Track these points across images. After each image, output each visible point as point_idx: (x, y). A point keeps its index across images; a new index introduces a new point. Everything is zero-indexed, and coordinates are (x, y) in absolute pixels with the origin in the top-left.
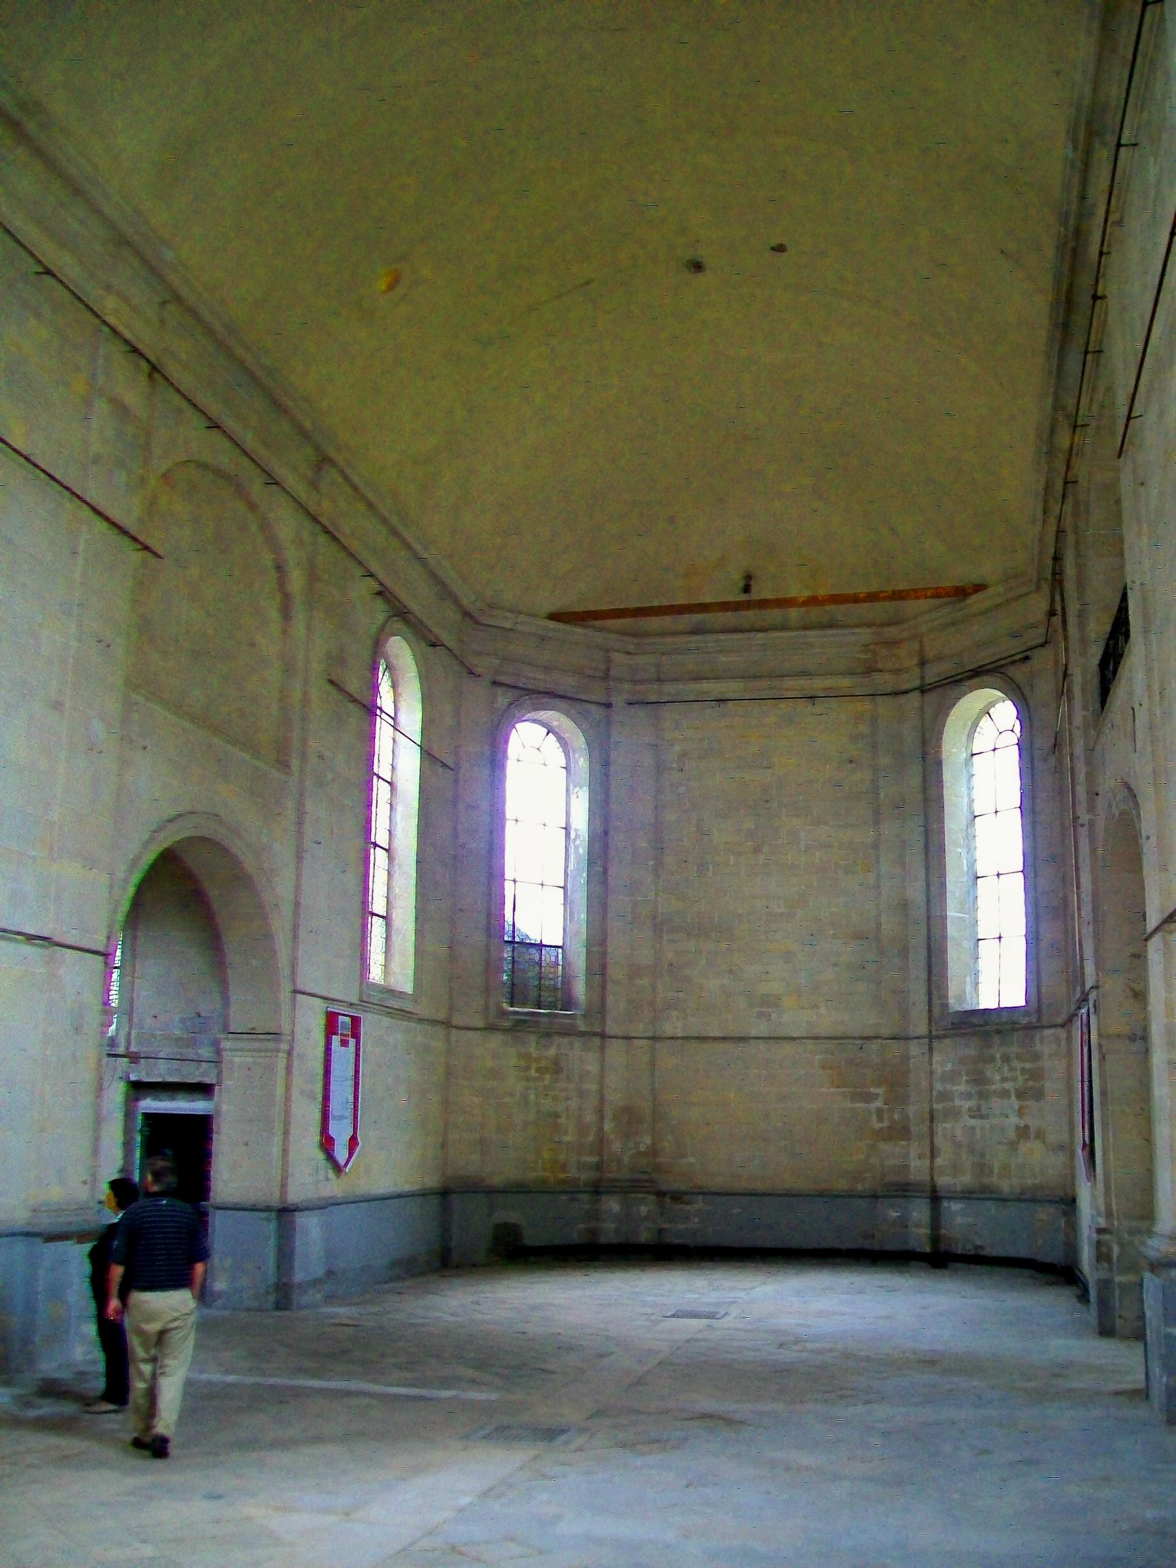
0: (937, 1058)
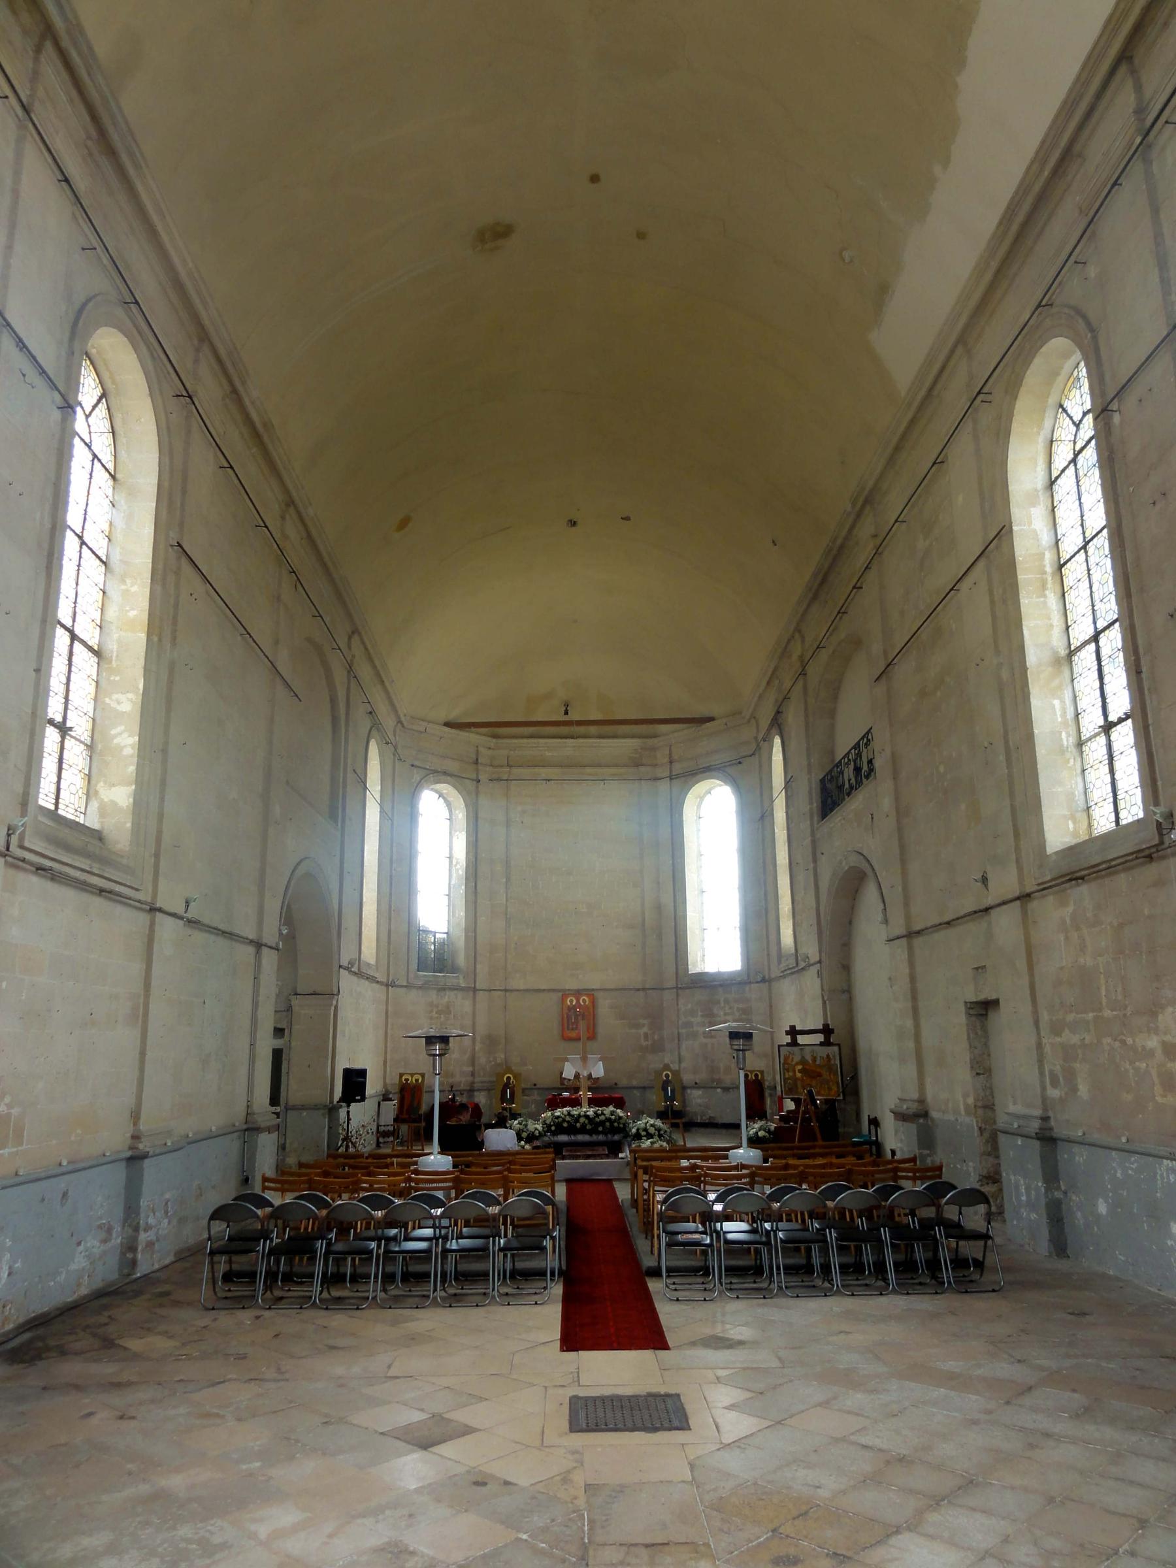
0: (681, 1001)
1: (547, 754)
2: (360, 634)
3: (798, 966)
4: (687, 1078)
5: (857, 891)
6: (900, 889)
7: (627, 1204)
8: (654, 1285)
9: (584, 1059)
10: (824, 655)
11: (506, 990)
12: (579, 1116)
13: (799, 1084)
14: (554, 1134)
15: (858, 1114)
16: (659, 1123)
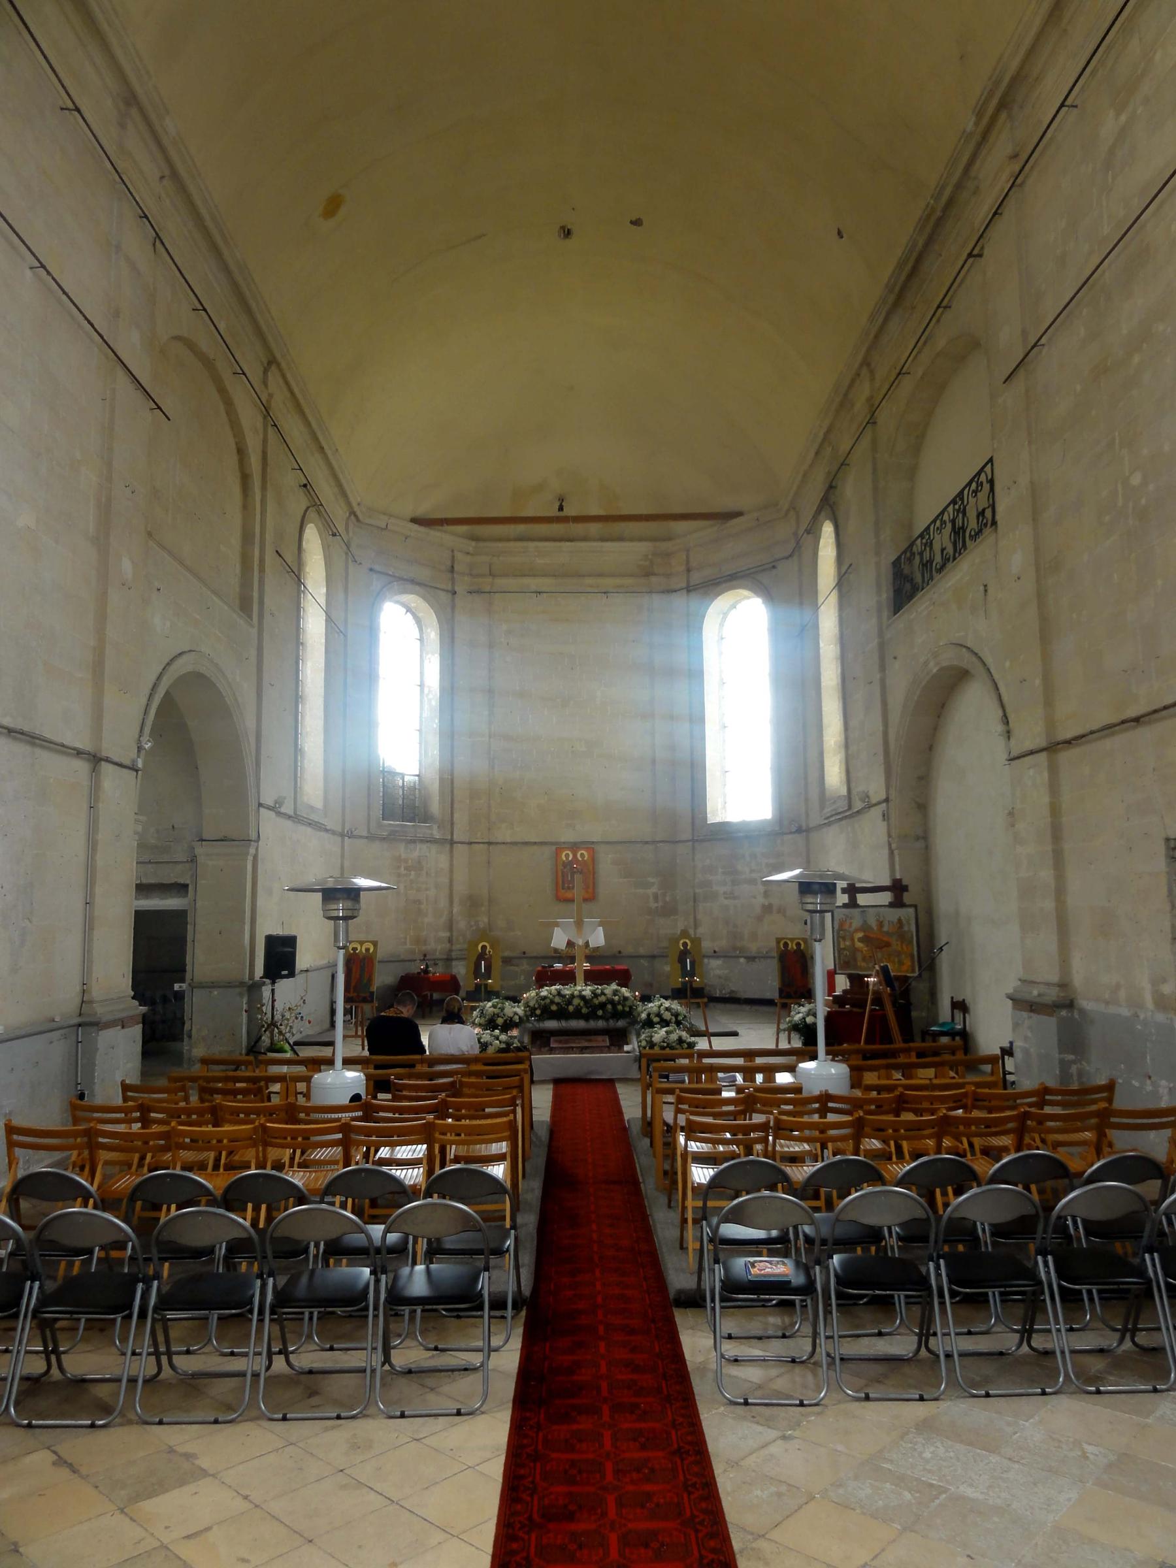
1: (539, 561)
2: (278, 365)
3: (850, 810)
4: (707, 945)
5: (943, 706)
6: (1038, 682)
7: (635, 1130)
8: (696, 1342)
9: (579, 924)
10: (907, 385)
11: (490, 843)
12: (573, 996)
13: (859, 957)
14: (541, 1018)
15: (933, 994)
16: (675, 1006)
